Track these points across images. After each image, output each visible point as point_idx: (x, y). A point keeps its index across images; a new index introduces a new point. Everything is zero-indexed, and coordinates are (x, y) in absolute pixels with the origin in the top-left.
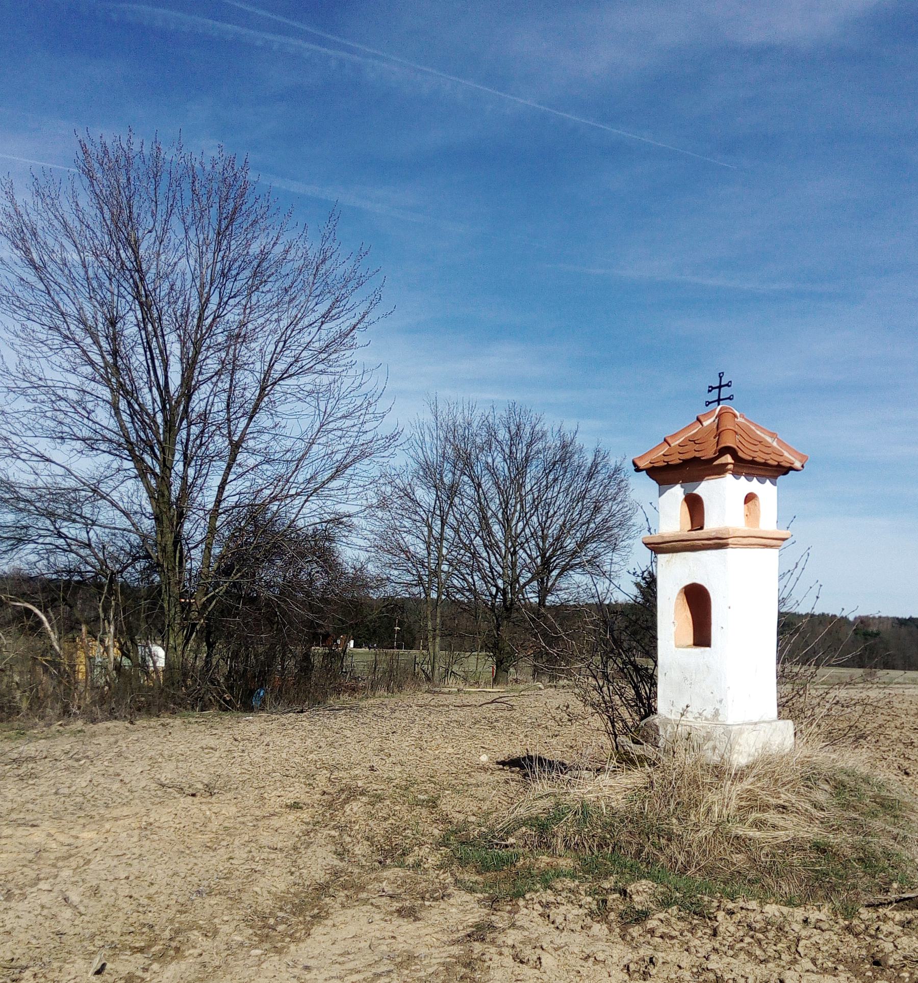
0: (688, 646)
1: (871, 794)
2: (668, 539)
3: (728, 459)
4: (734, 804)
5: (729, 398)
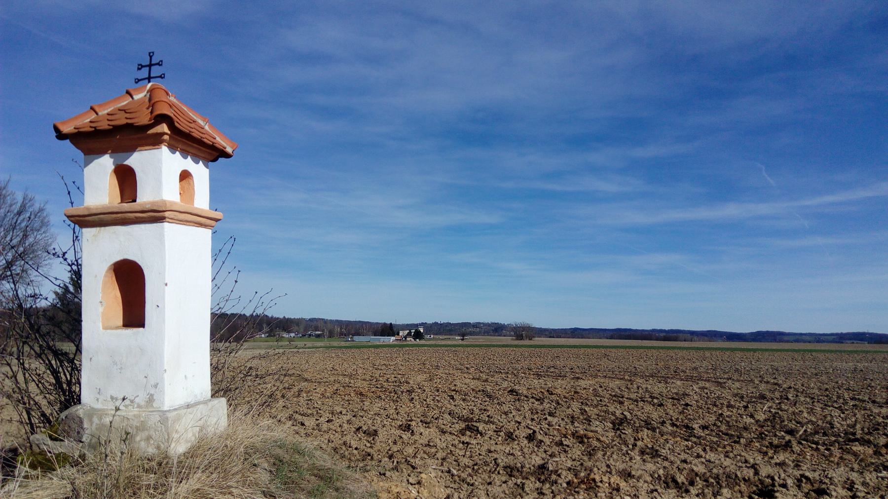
0: (117, 328)
2: (95, 212)
3: (164, 128)
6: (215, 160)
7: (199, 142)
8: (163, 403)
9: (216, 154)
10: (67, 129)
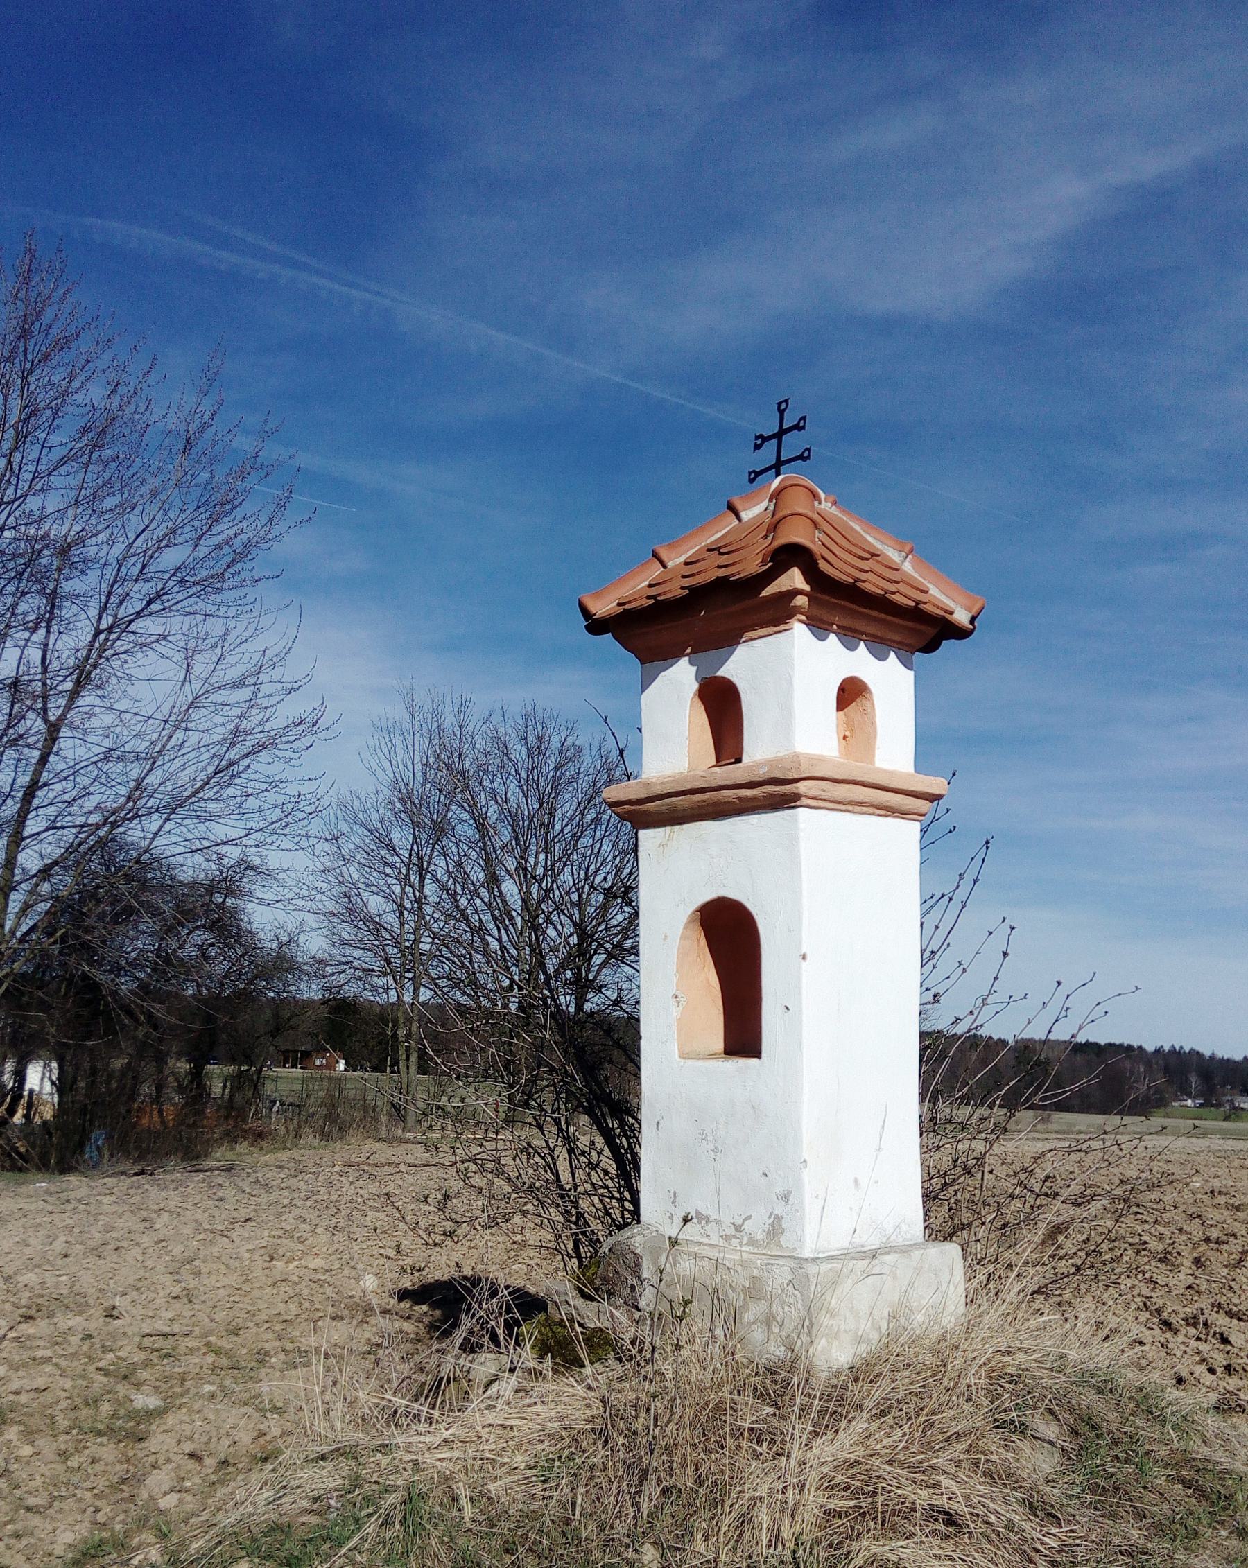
0: (712, 1056)
1: (1164, 1452)
3: (795, 578)
4: (813, 1501)
5: (801, 457)
6: (931, 647)
7: (881, 604)
8: (801, 1239)
9: (931, 631)
10: (603, 607)
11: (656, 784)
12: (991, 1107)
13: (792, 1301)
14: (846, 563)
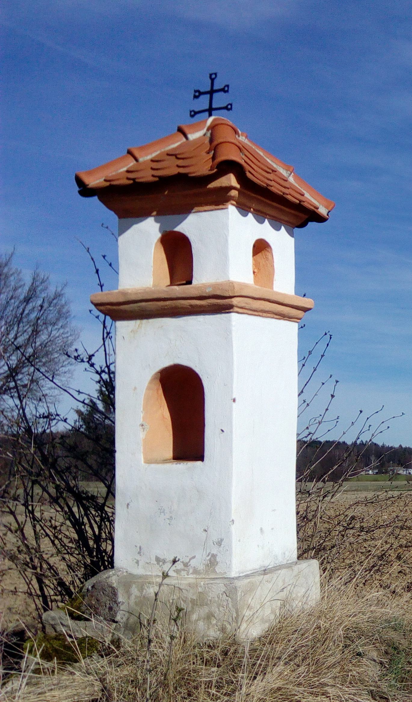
0: (165, 461)
2: (133, 298)
3: (231, 180)
5: (226, 108)
6: (303, 225)
8: (229, 567)
10: (94, 181)
11: (131, 294)
12: (324, 481)
13: (225, 604)
14: (260, 174)
